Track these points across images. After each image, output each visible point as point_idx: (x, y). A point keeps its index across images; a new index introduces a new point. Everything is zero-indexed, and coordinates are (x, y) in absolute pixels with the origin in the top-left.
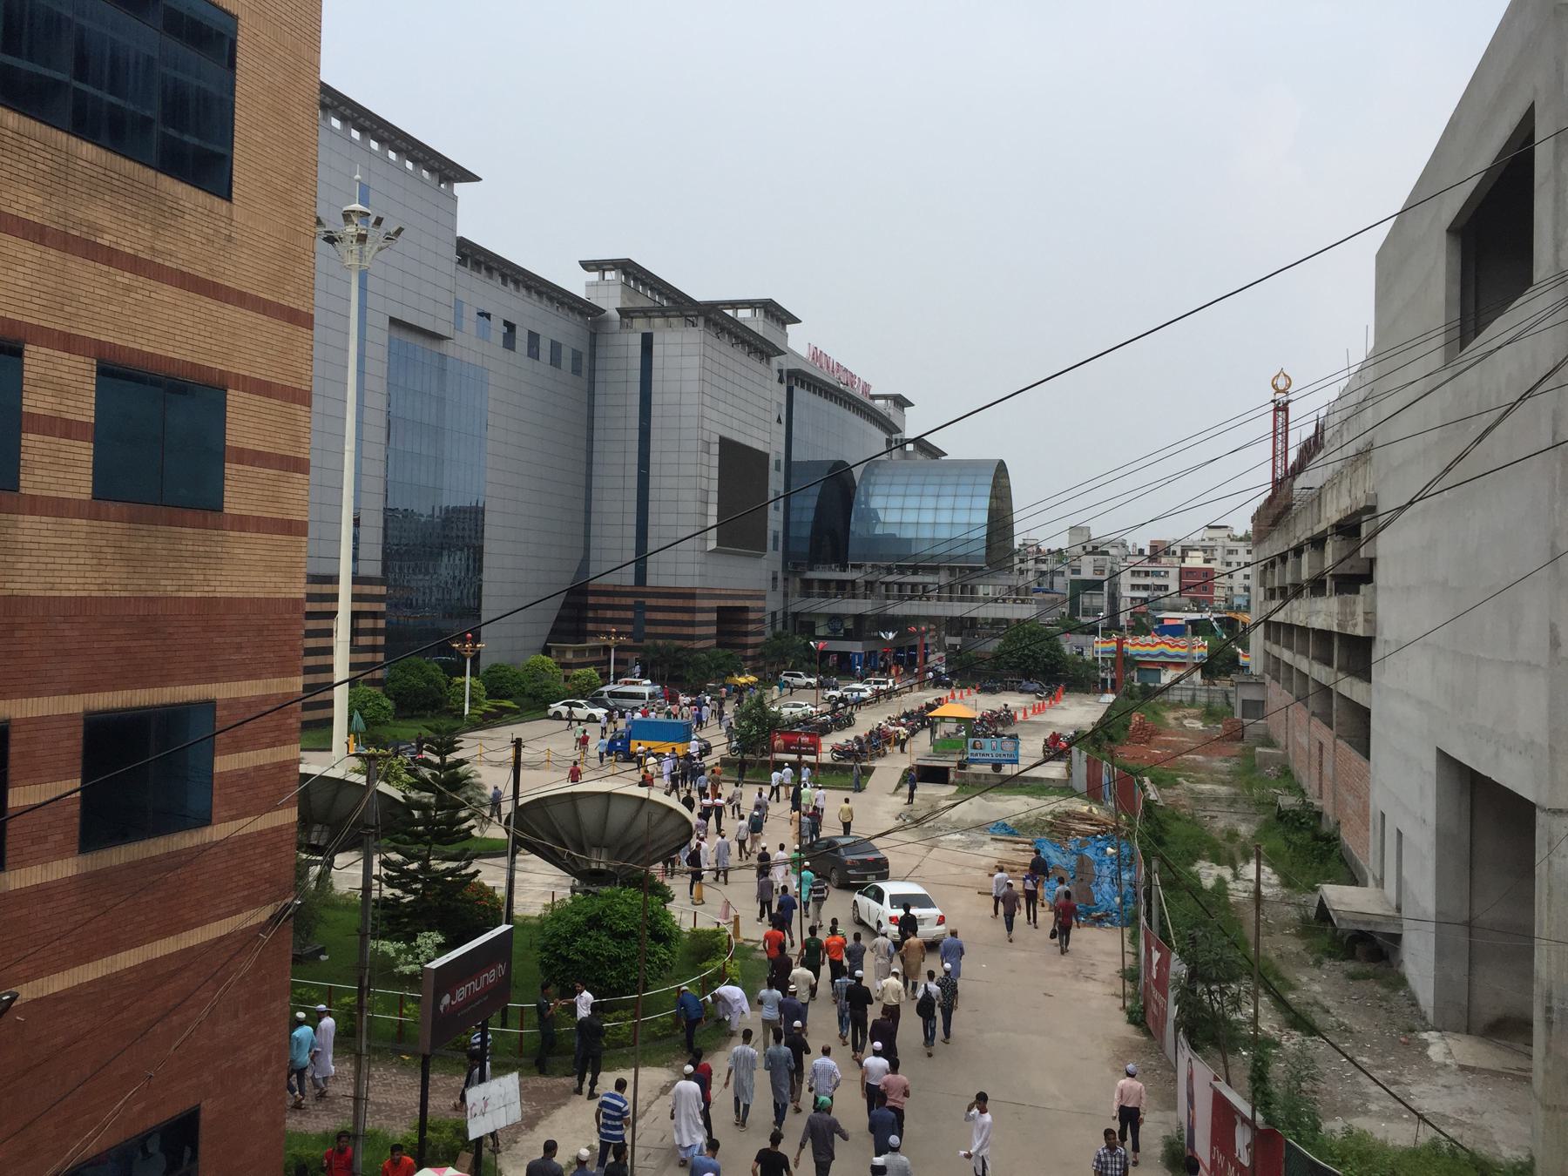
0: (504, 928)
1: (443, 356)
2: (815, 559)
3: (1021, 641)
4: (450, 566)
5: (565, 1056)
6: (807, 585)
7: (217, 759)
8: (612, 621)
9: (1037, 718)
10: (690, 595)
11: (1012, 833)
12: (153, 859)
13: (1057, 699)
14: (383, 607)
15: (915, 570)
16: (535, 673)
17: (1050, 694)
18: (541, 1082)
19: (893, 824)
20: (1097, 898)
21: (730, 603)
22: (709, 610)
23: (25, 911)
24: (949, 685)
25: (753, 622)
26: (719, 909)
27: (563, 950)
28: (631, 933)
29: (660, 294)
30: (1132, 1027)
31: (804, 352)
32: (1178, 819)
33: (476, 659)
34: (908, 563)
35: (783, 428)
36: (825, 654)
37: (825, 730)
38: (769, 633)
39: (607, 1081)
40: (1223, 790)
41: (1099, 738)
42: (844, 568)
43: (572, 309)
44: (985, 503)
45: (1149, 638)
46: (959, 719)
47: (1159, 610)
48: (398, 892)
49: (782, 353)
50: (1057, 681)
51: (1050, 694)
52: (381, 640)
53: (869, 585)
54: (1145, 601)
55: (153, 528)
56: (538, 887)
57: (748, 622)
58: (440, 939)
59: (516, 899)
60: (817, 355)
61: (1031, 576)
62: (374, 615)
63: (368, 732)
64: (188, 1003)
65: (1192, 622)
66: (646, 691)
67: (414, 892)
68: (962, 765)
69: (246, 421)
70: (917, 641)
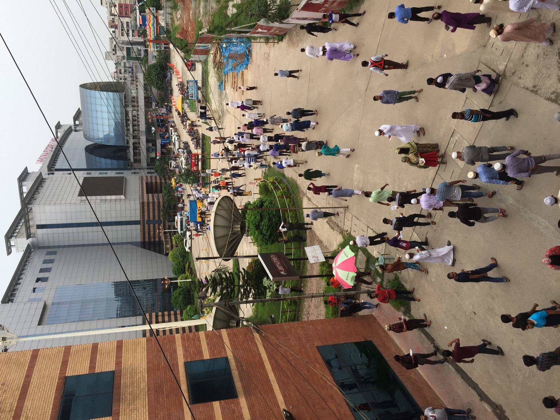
0: (259, 257)
1: (53, 304)
2: (126, 158)
3: (152, 79)
4: (139, 293)
5: (300, 233)
6: (136, 161)
7: (205, 358)
8: (154, 232)
9: (181, 73)
10: (143, 204)
11: (222, 83)
12: (239, 374)
13: (173, 66)
14: (154, 314)
15: (127, 120)
16: (175, 258)
17: (171, 69)
18: (308, 240)
20: (242, 52)
21: (145, 189)
23: (257, 412)
24: (171, 107)
25: (151, 180)
26: (252, 186)
27: (267, 237)
28: (261, 214)
29: (19, 223)
30: (284, 40)
31: (40, 165)
32: (213, 21)
33: (171, 279)
34: (125, 123)
36: (162, 153)
37: (189, 152)
38: (156, 174)
39: (307, 220)
40: (202, 4)
41: (186, 48)
42: (128, 147)
43: (29, 257)
44: (97, 93)
45: (147, 30)
46: (183, 103)
47: (136, 26)
48: (251, 294)
49: (41, 174)
50: (166, 66)
51: (171, 69)
52: (166, 313)
53: (134, 137)
54: (133, 31)
55: (121, 393)
56: (248, 247)
57: (152, 183)
58: (265, 278)
59: (252, 254)
60: (41, 160)
61: (127, 76)
62: (157, 316)
63: (198, 313)
64: (285, 355)
65: (140, 12)
66: (179, 217)
67: (250, 289)
68: (199, 101)
69: (79, 367)
70: (155, 119)
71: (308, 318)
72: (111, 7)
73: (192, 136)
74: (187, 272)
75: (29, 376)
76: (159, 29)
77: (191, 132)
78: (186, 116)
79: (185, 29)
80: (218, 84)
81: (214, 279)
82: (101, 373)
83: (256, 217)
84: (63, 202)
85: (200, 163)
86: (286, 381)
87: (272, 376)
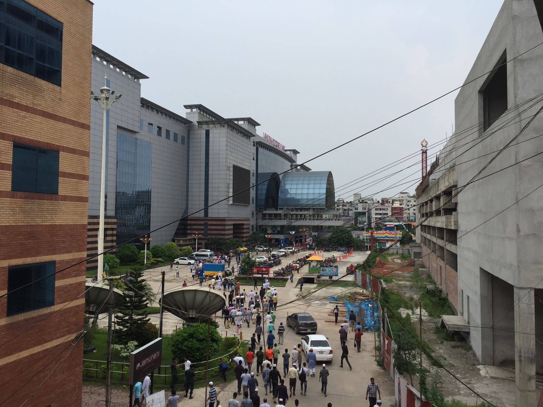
0: (159, 339)
1: (136, 139)
2: (267, 207)
4: (139, 211)
6: (264, 215)
9: (344, 260)
10: (224, 220)
11: (336, 300)
12: (33, 318)
14: (115, 226)
15: (301, 210)
16: (169, 248)
17: (348, 251)
19: (295, 298)
20: (366, 322)
21: (237, 222)
22: (231, 225)
24: (313, 249)
27: (180, 346)
28: (204, 339)
30: (379, 367)
31: (262, 135)
34: (299, 207)
35: (255, 162)
36: (271, 240)
37: (271, 266)
38: (251, 233)
40: (408, 283)
41: (366, 266)
42: (277, 209)
43: (181, 122)
44: (325, 186)
46: (317, 261)
48: (121, 327)
50: (351, 247)
51: (348, 251)
52: (115, 238)
53: (285, 215)
54: (380, 219)
55: (33, 200)
56: (171, 324)
57: (244, 229)
58: (136, 343)
59: (163, 328)
60: (266, 136)
61: (341, 211)
62: (112, 229)
63: (110, 270)
65: (396, 226)
66: (209, 254)
67: (127, 327)
69: (66, 162)
70: (302, 234)
71: (86, 393)
72: (400, 201)
73: (286, 269)
74: (154, 259)
75: (64, 120)
76: (383, 241)
77: (290, 268)
78: (305, 264)
79: (385, 266)
80: (335, 297)
81: (142, 288)
82: (58, 182)
83: (201, 334)
84: (227, 154)
85: (260, 276)
86: (17, 370)
87: (25, 354)
